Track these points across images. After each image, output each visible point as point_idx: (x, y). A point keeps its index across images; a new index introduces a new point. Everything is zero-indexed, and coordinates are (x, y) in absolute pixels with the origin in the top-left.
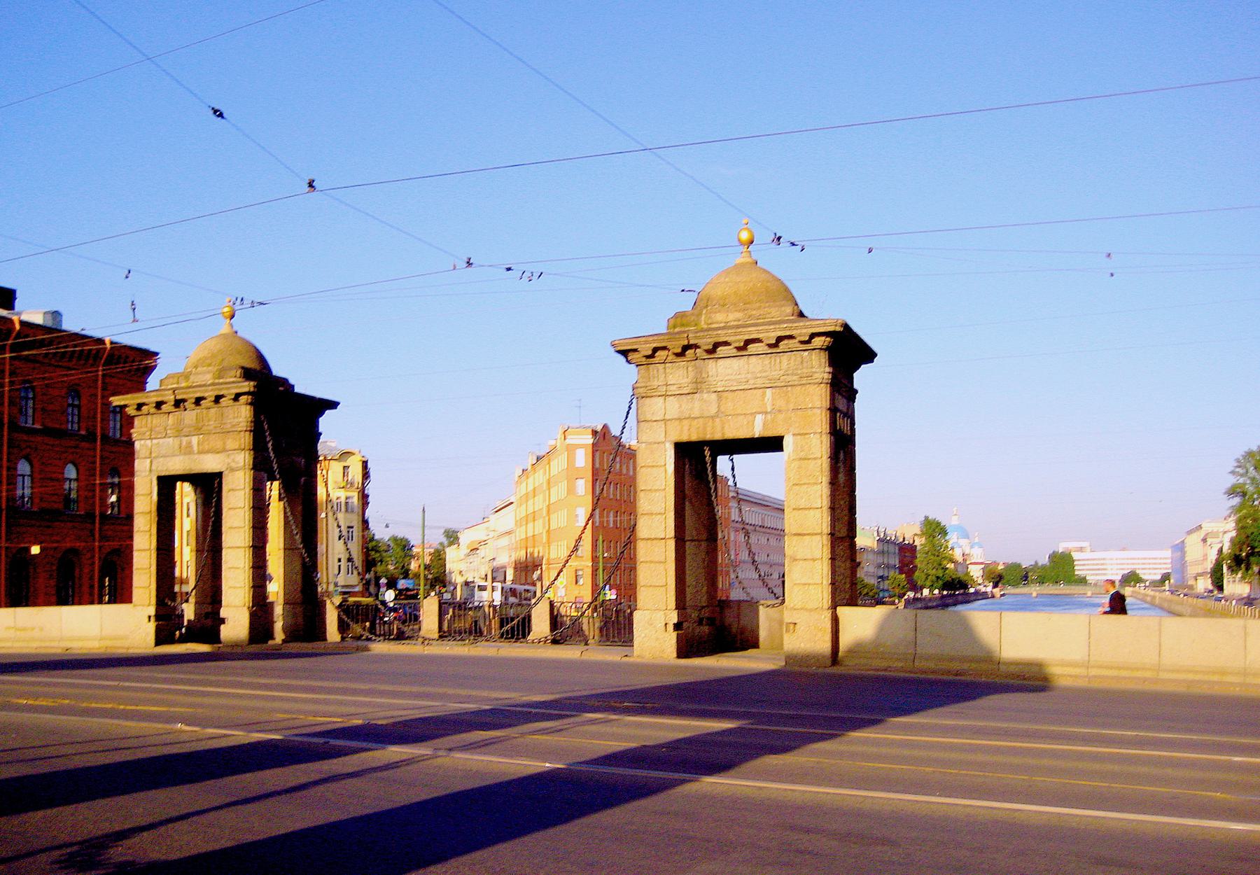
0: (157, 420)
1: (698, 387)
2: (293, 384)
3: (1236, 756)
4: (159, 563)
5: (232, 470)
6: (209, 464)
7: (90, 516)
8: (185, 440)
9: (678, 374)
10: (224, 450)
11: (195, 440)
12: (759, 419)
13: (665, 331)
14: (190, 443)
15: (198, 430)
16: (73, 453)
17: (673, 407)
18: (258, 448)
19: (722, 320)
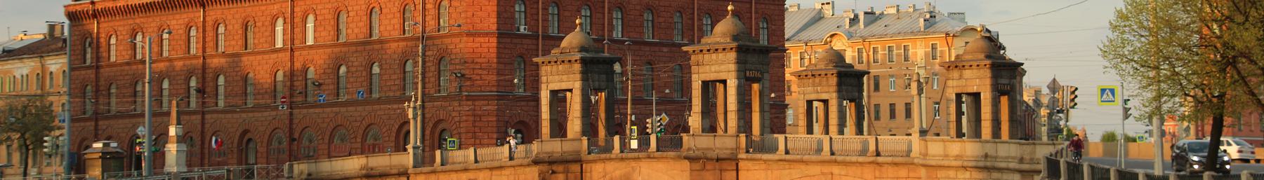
0: (549, 68)
1: (961, 77)
2: (1017, 59)
3: (969, 121)
4: (748, 110)
5: (831, 99)
6: (824, 96)
7: (535, 37)
8: (815, 88)
9: (956, 74)
10: (829, 92)
11: (819, 88)
12: (975, 87)
13: (824, 68)
14: (817, 89)
15: (820, 85)
16: (1032, 161)
17: (955, 83)
18: (839, 91)
19: (83, 91)
